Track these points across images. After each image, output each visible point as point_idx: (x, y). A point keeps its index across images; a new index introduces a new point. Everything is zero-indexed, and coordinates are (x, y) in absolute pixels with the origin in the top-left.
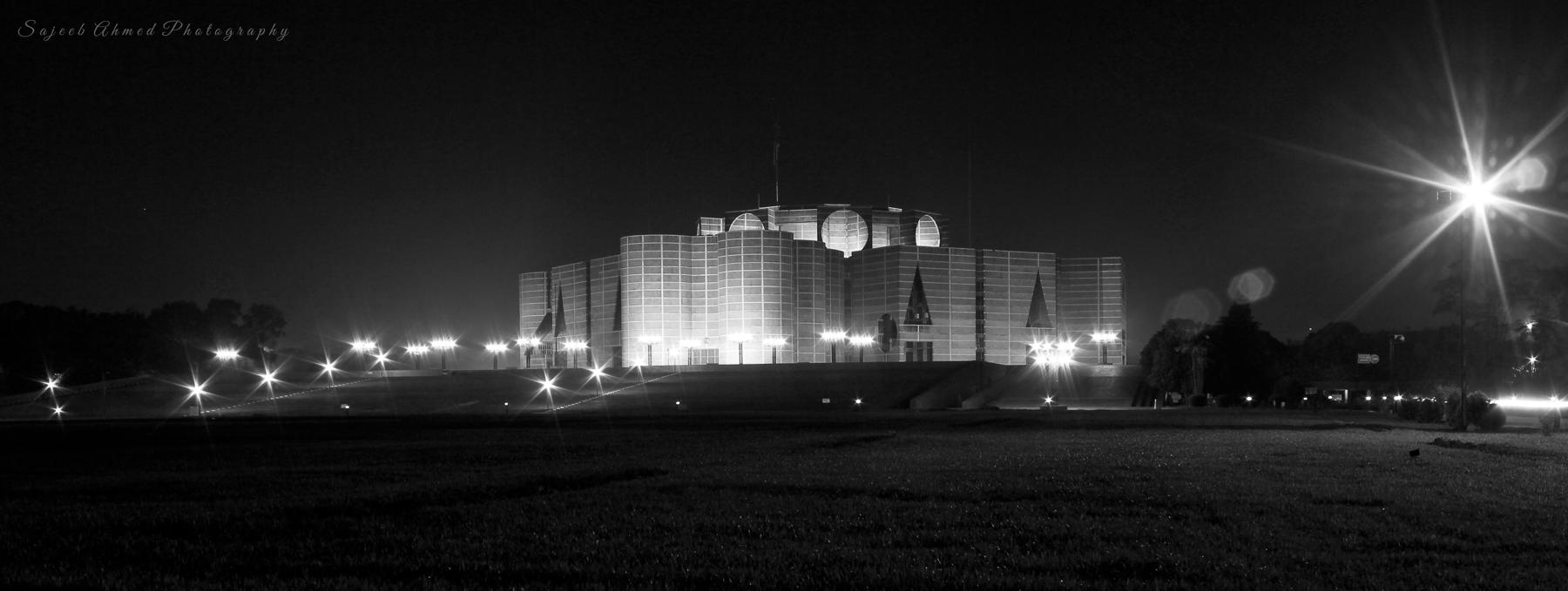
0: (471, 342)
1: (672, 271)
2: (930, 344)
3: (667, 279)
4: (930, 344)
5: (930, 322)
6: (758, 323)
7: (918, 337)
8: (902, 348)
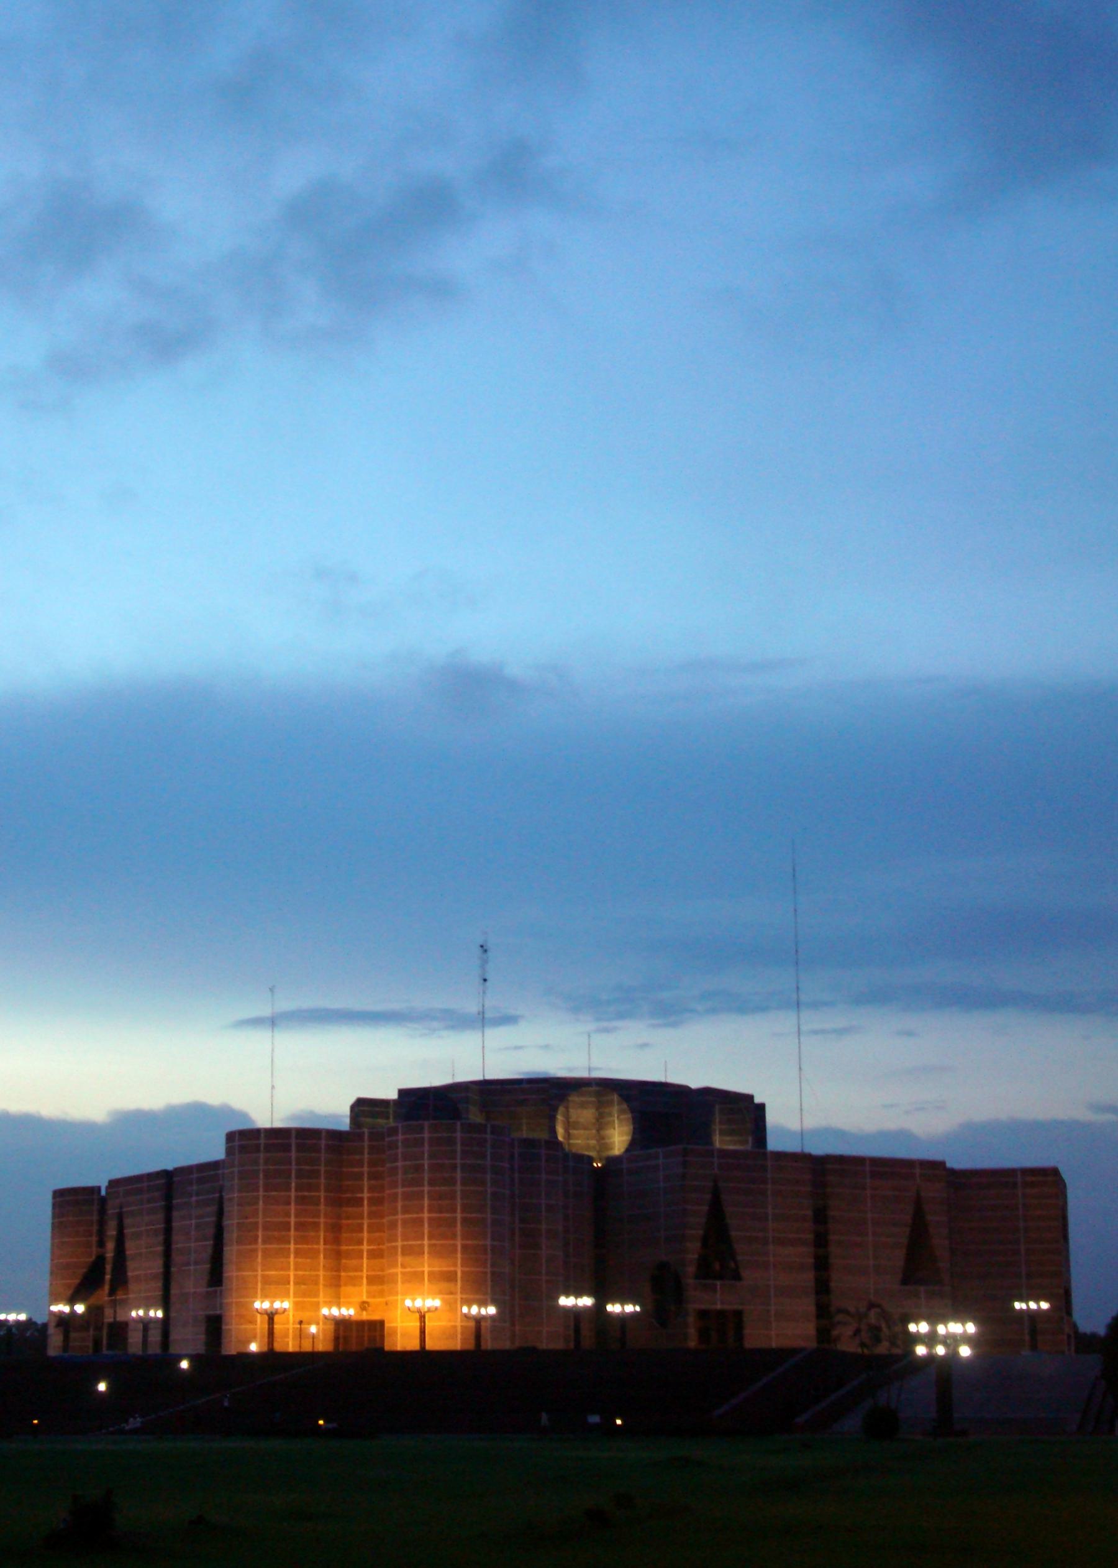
0: (599, 1307)
1: (310, 1188)
2: (738, 1314)
3: (407, 1197)
4: (738, 1314)
5: (737, 1277)
6: (450, 1277)
7: (719, 1300)
8: (691, 1319)
